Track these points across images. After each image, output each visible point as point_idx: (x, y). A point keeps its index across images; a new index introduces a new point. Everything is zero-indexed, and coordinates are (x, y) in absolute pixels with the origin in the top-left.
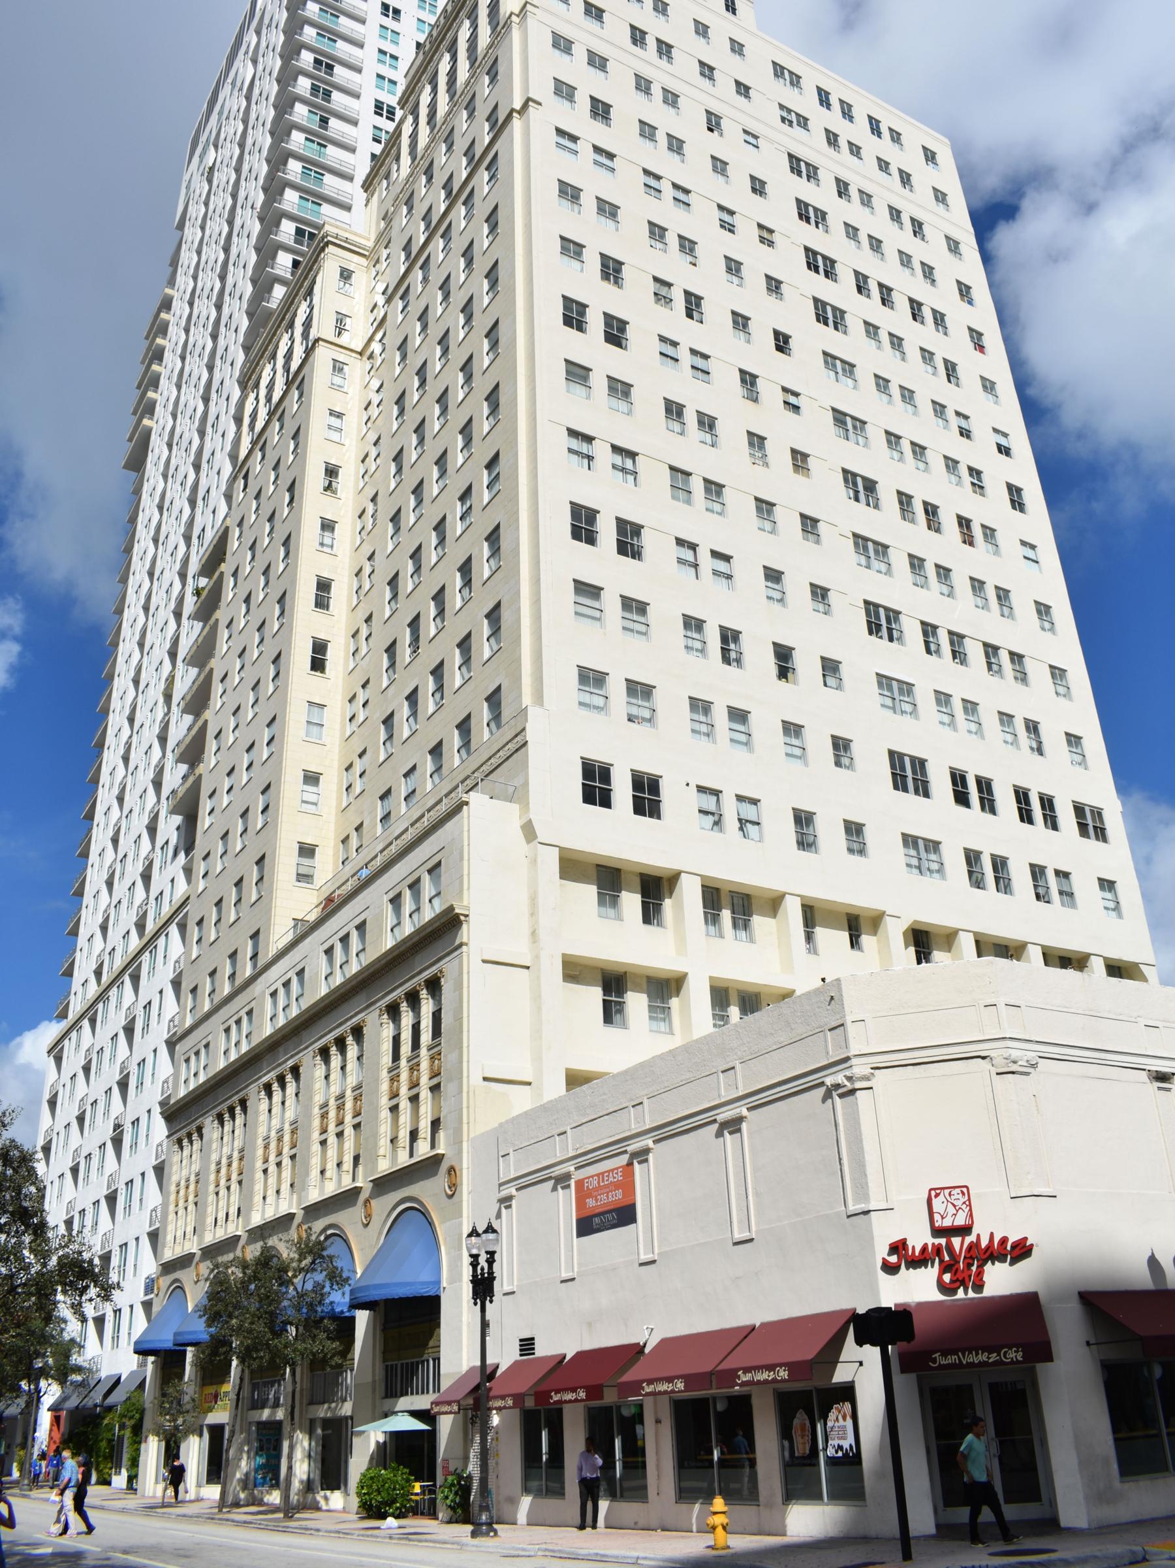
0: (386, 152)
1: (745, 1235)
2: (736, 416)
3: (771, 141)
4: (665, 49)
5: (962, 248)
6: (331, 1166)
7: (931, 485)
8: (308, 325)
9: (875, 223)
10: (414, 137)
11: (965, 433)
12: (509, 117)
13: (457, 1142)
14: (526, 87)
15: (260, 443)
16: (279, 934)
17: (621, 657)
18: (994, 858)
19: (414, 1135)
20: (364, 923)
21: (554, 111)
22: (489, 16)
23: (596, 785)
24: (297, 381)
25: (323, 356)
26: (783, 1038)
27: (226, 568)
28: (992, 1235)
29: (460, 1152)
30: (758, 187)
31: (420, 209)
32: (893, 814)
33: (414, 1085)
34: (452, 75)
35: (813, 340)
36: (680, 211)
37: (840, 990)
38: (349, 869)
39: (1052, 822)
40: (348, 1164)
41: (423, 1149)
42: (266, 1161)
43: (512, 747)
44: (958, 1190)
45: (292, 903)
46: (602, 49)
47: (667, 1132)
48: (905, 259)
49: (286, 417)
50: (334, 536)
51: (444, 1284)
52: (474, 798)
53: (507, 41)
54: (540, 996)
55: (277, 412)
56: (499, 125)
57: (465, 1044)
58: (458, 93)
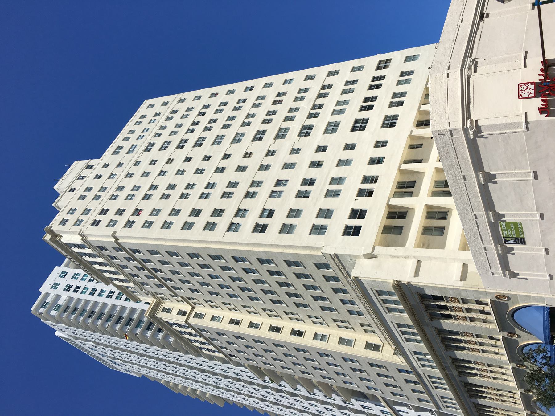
0: (127, 293)
1: (532, 175)
2: (230, 175)
3: (139, 157)
4: (103, 189)
5: (183, 98)
6: (493, 349)
7: (261, 113)
8: (180, 326)
9: (171, 125)
10: (120, 280)
11: (244, 101)
12: (119, 244)
13: (486, 294)
14: (108, 236)
15: (220, 349)
16: (400, 361)
17: (309, 219)
18: (393, 97)
19: (482, 312)
20: (428, 376)
21: (119, 228)
22: (81, 248)
23: (353, 231)
24: (200, 331)
25: (193, 321)
26: (453, 155)
27: (263, 367)
28: (539, 75)
29: (490, 293)
30: (153, 162)
31: (145, 280)
32: (374, 130)
33: (476, 343)
34: (100, 264)
35: (207, 148)
36: (158, 189)
37: (436, 131)
38: (377, 330)
39: (382, 78)
40: (493, 342)
41: (488, 309)
42: (489, 377)
43: (336, 260)
44: (520, 88)
45: (387, 354)
46: (99, 210)
47: (489, 204)
48: (185, 116)
49: (212, 338)
50: (256, 323)
51: (545, 305)
52: (353, 274)
53: (91, 242)
54: (430, 257)
55: (210, 341)
56: (120, 248)
57: (446, 287)
58: (107, 262)
